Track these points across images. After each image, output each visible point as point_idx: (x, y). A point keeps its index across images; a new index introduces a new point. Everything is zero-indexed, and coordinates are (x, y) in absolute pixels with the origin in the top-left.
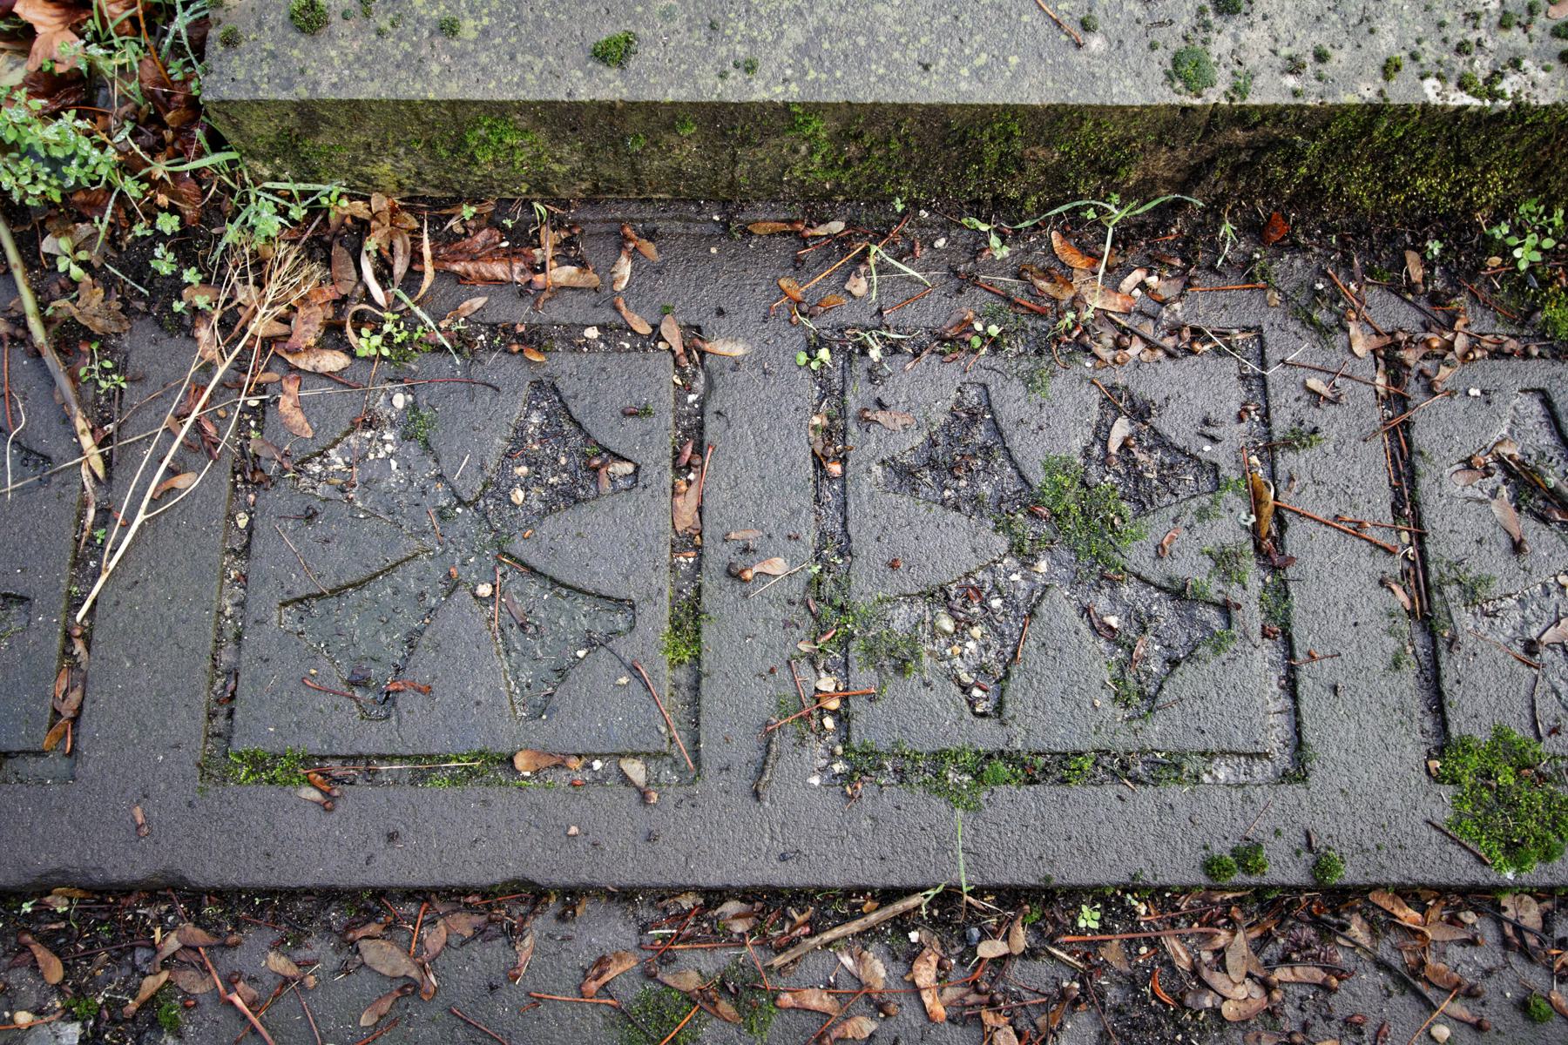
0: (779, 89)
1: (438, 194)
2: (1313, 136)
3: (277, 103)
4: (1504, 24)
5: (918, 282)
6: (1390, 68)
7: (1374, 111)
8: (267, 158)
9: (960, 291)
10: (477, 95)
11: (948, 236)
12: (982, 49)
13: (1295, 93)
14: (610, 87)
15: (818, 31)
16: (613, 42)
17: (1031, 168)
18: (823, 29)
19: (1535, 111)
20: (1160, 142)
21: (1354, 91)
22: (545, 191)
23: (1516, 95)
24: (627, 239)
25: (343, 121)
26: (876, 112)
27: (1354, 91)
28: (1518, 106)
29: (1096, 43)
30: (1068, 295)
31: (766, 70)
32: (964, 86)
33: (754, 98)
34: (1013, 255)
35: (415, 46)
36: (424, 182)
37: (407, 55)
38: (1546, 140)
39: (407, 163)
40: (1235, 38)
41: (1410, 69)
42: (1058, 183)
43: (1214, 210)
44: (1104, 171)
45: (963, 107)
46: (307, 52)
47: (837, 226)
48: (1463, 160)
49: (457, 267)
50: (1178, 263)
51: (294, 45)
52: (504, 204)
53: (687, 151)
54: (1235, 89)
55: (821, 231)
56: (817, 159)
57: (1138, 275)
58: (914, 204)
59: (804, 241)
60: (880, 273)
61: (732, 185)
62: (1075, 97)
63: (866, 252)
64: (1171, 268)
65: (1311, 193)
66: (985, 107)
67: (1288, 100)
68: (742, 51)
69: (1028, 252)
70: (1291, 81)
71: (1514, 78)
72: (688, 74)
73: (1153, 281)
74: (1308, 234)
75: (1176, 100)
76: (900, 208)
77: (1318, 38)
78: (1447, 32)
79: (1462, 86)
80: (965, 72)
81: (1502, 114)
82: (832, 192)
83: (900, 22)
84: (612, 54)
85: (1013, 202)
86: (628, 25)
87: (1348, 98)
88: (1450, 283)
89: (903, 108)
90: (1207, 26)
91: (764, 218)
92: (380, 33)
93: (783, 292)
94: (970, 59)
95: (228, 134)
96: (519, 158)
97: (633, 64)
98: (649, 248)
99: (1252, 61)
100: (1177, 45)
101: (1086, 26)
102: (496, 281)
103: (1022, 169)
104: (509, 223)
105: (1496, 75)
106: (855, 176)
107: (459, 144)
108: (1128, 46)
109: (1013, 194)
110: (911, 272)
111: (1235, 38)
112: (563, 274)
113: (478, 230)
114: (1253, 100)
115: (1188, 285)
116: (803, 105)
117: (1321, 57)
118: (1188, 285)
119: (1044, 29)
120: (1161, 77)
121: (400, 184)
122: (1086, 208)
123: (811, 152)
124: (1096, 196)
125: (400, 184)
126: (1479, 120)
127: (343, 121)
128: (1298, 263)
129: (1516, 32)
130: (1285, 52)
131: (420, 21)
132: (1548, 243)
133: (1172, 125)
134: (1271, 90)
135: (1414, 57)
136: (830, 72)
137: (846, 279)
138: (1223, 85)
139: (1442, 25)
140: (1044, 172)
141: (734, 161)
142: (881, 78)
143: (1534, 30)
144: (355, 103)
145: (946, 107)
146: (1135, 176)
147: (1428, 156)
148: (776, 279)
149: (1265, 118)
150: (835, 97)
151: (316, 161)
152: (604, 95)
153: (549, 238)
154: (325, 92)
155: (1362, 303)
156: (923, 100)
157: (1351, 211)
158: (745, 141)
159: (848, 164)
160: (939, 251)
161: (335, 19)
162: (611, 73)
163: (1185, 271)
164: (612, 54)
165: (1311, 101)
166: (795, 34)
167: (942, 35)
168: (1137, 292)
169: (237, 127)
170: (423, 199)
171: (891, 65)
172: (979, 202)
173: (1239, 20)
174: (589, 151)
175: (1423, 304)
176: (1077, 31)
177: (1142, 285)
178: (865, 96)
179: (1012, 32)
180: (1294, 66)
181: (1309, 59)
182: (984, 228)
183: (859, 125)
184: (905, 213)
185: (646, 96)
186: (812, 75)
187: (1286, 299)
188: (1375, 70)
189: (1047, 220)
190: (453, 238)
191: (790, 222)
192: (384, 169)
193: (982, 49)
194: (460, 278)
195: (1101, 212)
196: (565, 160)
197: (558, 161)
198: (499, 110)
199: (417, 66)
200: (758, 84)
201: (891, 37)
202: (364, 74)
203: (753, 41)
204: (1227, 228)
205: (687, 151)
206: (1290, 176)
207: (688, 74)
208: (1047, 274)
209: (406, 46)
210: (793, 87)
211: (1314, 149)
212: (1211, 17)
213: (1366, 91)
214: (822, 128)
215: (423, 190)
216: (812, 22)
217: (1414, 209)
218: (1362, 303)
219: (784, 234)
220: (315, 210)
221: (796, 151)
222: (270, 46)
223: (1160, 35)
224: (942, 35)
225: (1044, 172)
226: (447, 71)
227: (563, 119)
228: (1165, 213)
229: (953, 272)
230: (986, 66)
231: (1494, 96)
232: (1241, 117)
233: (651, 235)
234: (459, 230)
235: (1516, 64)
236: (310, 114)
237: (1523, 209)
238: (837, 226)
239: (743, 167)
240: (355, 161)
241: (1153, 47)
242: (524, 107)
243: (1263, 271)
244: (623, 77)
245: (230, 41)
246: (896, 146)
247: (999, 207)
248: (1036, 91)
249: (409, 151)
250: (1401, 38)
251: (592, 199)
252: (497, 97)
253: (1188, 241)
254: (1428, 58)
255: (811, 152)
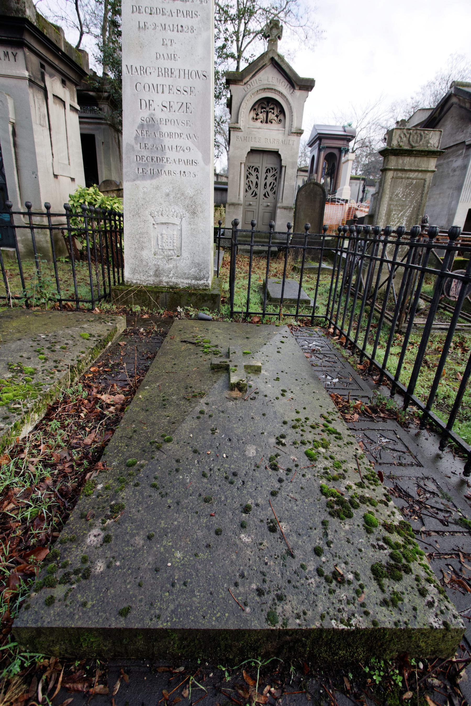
0: (165, 624)
1: (70, 657)
2: (307, 638)
3: (31, 628)
4: (348, 603)
5: (204, 691)
6: (322, 617)
7: (321, 631)
8: (25, 645)
9: (216, 695)
10: (85, 626)
11: (213, 672)
12: (219, 611)
13: (299, 625)
14: (121, 623)
15: (178, 606)
16: (125, 609)
17: (234, 649)
18: (179, 605)
19: (362, 630)
20: (267, 640)
21: (314, 624)
22: (101, 656)
23: (356, 625)
24: (121, 674)
25: (48, 633)
26: (190, 631)
27: (314, 624)
28: (357, 628)
29: (248, 609)
30: (248, 696)
31: (162, 618)
32: (213, 623)
33: (158, 627)
34: (232, 679)
35: (74, 610)
36: (67, 653)
37: (71, 613)
38: (368, 638)
39: (63, 647)
40: (283, 607)
41: (327, 617)
42: (243, 654)
43: (287, 661)
44: (254, 650)
45: (213, 630)
46: (45, 612)
47: (182, 669)
48: (349, 645)
49: (67, 686)
50: (279, 682)
51: (43, 609)
52: (89, 660)
53: (140, 643)
54: (284, 623)
55: (177, 671)
56: (176, 646)
57: (268, 688)
58: (203, 661)
59: (172, 674)
60: (192, 687)
61: (153, 654)
62: (243, 627)
63: (189, 678)
64: (278, 684)
65: (312, 657)
66: (219, 630)
67: (297, 627)
68: (157, 612)
69: (236, 678)
70: (298, 621)
71: (354, 620)
72: (142, 619)
73: (273, 689)
74: (315, 670)
75: (269, 627)
76: (199, 662)
77: (303, 608)
78: (335, 605)
79: (342, 622)
80: (214, 618)
81: (354, 631)
82: (181, 656)
83: (199, 603)
84: (124, 613)
85: (232, 659)
86: (130, 604)
87: (313, 627)
88: (359, 689)
89: (198, 630)
90: (275, 604)
91: (162, 666)
92: (66, 606)
93: (163, 696)
94: (216, 614)
95: (16, 637)
96: (94, 645)
97: (128, 616)
98: (127, 677)
99: (288, 615)
100: (268, 610)
101: (246, 604)
102: (78, 691)
103: (231, 649)
104: (88, 667)
105: (349, 619)
106: (187, 651)
107: (78, 640)
108: (256, 609)
109: (231, 657)
110: (202, 687)
111: (283, 607)
112: (99, 688)
113: (78, 670)
114: (289, 627)
115: (283, 692)
116: (171, 629)
117: (305, 613)
118: (283, 692)
119: (235, 605)
120: (264, 620)
121: (60, 653)
122: (251, 662)
123: (174, 644)
124: (254, 658)
125: (60, 653)
126: (349, 633)
127: (48, 633)
128: (314, 682)
129: (351, 605)
130: (295, 612)
131: (78, 602)
132: (382, 674)
133: (270, 634)
134: (294, 624)
135: (328, 613)
136: (179, 619)
137: (182, 690)
138: (281, 623)
139: (333, 603)
140: (238, 649)
141: (153, 646)
142: (192, 621)
143: (356, 605)
144: (52, 628)
145: (208, 630)
146: (263, 651)
147: (340, 644)
148: (162, 690)
149: (293, 633)
150: (179, 627)
151: (39, 646)
152: (119, 626)
153: (99, 673)
154: (45, 625)
155: (334, 698)
156: (203, 628)
157: (326, 662)
158: (156, 640)
159: (184, 648)
160: (211, 678)
161: (56, 601)
162: (122, 619)
163: (282, 685)
164: (124, 613)
165: (304, 628)
166: (172, 607)
167: (209, 607)
168: (268, 695)
169: (19, 635)
170: (66, 658)
171: (196, 616)
172: (222, 660)
173: (283, 602)
174: (114, 643)
175: (353, 698)
176: (243, 606)
177: (269, 692)
178: (187, 627)
179: (226, 606)
180: (298, 617)
181: (302, 614)
182: (224, 669)
183: (187, 635)
184: (201, 664)
185: (130, 626)
186: (174, 619)
187: (313, 697)
188: (318, 618)
189: (241, 666)
190: (72, 673)
191: (169, 667)
192: (57, 648)
193: (219, 611)
194: (68, 689)
195: (256, 663)
196: (107, 646)
197: (105, 646)
198: (90, 630)
199: (71, 616)
200: (160, 622)
201: (196, 608)
202: (57, 619)
203: (161, 609)
204: (292, 668)
205: (140, 643)
206: (305, 651)
207: (142, 619)
208: (242, 688)
209: (72, 610)
210: (169, 624)
211: (308, 642)
212: (276, 601)
213: (317, 624)
214: (176, 636)
215: (67, 655)
216: (177, 602)
217: (343, 661)
218: (334, 698)
219: (167, 671)
220: (34, 663)
221: (170, 643)
222: (36, 609)
223: (264, 607)
224: (209, 607)
225: (238, 649)
226: (80, 618)
227: (106, 633)
228: (275, 662)
229: (215, 687)
230: (220, 617)
231: (351, 625)
232: (287, 632)
233: (128, 672)
234: (73, 670)
235: (353, 615)
236: (39, 631)
237: (372, 660)
238: (182, 669)
239: (156, 648)
240: (49, 646)
241: (262, 610)
242: (97, 629)
243: (304, 685)
244: (125, 620)
245: (27, 608)
246: (196, 642)
247: (228, 662)
248: (232, 625)
249: (64, 643)
250: (324, 607)
251: (114, 659)
252: (90, 627)
253: (282, 673)
254: (331, 613)
255: (174, 644)
